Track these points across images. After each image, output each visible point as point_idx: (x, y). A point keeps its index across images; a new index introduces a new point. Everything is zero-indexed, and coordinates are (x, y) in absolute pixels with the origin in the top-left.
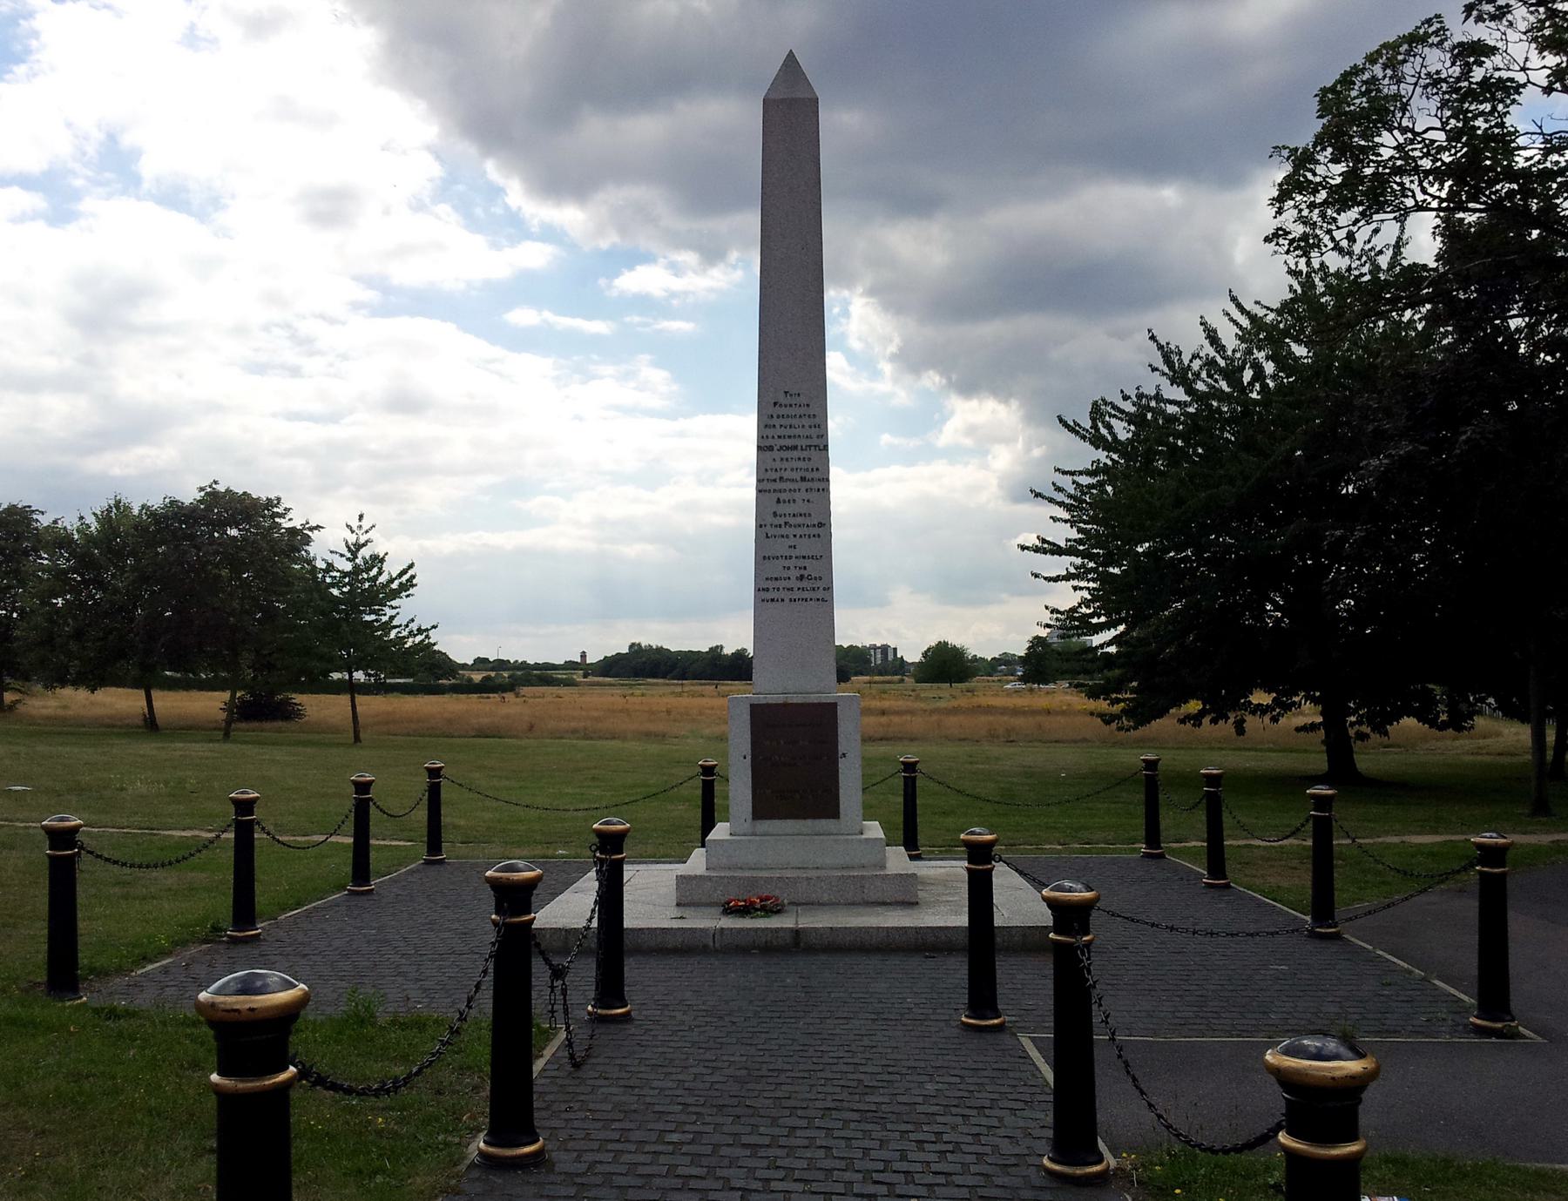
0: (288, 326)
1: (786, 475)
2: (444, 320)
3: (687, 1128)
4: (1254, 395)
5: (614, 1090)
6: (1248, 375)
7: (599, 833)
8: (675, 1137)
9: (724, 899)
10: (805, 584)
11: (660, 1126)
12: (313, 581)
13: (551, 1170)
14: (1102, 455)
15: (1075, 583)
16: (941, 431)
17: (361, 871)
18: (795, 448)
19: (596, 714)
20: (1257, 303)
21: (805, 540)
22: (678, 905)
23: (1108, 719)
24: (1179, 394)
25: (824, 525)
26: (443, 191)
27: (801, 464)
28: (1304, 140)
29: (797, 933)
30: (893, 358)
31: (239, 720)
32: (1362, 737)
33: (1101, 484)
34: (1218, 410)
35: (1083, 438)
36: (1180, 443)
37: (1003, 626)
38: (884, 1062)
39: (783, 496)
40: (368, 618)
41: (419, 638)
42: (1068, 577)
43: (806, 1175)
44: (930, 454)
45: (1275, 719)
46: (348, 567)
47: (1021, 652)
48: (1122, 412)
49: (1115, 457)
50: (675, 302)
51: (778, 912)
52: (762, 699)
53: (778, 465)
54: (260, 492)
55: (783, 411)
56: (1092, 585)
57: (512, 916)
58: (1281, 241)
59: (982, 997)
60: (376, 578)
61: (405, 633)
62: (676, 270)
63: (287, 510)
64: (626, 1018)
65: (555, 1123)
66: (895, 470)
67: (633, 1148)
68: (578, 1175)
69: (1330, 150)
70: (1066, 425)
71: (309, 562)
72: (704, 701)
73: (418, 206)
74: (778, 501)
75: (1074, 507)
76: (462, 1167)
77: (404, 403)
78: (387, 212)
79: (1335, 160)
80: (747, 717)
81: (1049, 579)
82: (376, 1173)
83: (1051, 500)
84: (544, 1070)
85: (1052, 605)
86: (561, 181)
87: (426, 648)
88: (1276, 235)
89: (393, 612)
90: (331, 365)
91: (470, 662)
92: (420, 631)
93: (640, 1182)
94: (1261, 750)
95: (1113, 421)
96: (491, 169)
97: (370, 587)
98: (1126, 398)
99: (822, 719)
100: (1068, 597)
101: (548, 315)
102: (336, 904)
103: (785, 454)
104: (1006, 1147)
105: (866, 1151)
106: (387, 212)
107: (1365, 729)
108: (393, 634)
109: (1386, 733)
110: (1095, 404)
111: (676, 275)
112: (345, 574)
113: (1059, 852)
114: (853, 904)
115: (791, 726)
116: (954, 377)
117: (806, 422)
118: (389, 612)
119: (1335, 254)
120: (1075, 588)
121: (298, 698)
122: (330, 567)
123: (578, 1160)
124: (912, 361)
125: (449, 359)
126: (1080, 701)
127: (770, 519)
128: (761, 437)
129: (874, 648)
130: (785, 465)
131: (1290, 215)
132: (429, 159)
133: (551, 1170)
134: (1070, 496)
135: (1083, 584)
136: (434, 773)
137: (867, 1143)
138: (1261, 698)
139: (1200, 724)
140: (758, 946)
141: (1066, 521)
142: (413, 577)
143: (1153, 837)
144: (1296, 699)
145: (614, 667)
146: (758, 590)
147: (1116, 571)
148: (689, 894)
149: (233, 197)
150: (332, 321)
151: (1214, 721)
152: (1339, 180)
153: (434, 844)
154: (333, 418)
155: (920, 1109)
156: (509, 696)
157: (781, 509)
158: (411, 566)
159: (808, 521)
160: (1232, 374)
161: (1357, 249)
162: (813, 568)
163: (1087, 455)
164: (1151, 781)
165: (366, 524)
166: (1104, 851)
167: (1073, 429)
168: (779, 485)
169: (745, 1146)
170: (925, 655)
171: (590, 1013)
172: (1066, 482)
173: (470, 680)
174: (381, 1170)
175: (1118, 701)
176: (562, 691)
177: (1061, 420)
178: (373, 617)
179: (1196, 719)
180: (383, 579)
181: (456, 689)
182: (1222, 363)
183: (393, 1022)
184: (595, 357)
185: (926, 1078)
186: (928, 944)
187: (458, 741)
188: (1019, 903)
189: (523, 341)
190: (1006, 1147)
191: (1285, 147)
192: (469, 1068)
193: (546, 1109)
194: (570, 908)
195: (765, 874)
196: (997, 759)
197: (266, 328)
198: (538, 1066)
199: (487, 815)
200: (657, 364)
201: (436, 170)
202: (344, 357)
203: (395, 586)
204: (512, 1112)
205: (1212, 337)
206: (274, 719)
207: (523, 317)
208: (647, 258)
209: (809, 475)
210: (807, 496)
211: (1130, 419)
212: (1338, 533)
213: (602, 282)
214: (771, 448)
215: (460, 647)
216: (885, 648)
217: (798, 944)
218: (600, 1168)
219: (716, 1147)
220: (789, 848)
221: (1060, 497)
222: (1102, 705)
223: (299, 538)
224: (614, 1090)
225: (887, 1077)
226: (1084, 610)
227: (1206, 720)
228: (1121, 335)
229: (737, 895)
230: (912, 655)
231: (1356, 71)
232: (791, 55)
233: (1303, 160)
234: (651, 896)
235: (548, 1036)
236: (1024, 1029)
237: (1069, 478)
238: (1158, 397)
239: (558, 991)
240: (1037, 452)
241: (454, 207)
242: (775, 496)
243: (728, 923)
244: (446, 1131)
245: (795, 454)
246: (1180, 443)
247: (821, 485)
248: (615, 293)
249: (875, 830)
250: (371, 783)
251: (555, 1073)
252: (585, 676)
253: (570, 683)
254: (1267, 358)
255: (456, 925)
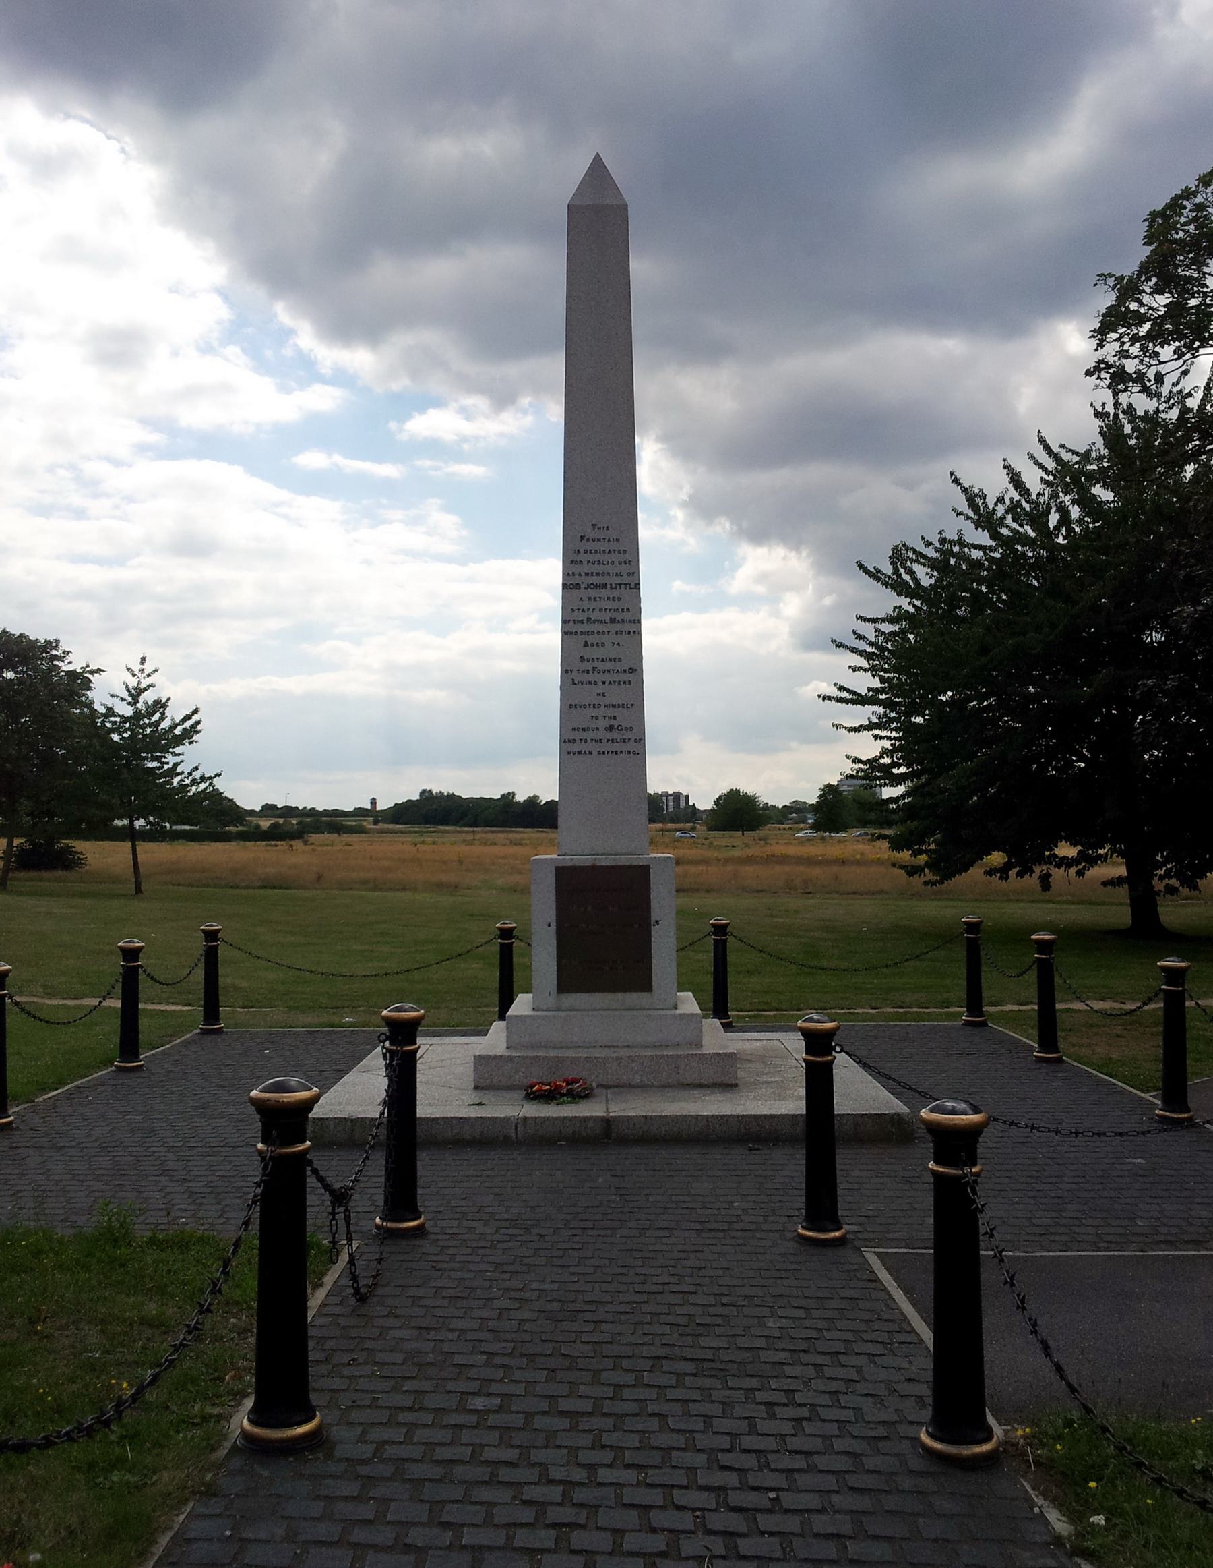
0: (72, 467)
2: (231, 462)
3: (495, 1388)
4: (1060, 540)
5: (404, 1333)
6: (1054, 519)
7: (389, 1022)
8: (479, 1403)
9: (527, 1082)
11: (462, 1386)
12: (93, 725)
13: (329, 1456)
14: (904, 602)
15: (877, 732)
16: (733, 578)
17: (130, 1044)
18: (604, 586)
19: (386, 863)
20: (1062, 446)
22: (476, 1088)
23: (912, 871)
24: (984, 538)
25: (636, 670)
26: (233, 332)
27: (609, 604)
28: (1129, 268)
29: (607, 1122)
30: (684, 505)
31: (17, 869)
32: (1171, 890)
33: (903, 632)
34: (1024, 555)
35: (885, 584)
36: (984, 589)
37: (793, 775)
38: (716, 1289)
39: (590, 639)
40: (150, 765)
41: (203, 786)
42: (871, 726)
43: (639, 1458)
44: (723, 601)
45: (1080, 873)
46: (128, 711)
47: (813, 800)
48: (925, 557)
49: (918, 603)
50: (466, 447)
51: (586, 1097)
52: (568, 861)
53: (586, 604)
54: (38, 634)
55: (590, 546)
56: (894, 734)
57: (283, 1145)
58: (1103, 375)
59: (821, 1204)
60: (158, 723)
61: (187, 782)
62: (467, 414)
63: (67, 653)
64: (420, 1231)
65: (337, 1383)
66: (686, 617)
67: (428, 1418)
68: (363, 1462)
69: (1154, 280)
70: (866, 571)
71: (89, 705)
72: (495, 850)
73: (206, 349)
74: (586, 644)
75: (876, 658)
76: (222, 1453)
77: (191, 546)
78: (175, 353)
79: (1158, 290)
80: (551, 880)
81: (851, 730)
82: (113, 1467)
83: (853, 650)
84: (323, 1305)
85: (854, 754)
86: (348, 325)
87: (216, 796)
88: (1097, 369)
89: (177, 759)
90: (117, 507)
91: (258, 809)
92: (203, 779)
93: (438, 1472)
94: (1059, 902)
95: (916, 567)
96: (283, 313)
97: (152, 734)
98: (928, 544)
99: (634, 882)
100: (869, 747)
101: (337, 458)
102: (102, 1083)
103: (592, 593)
104: (872, 1412)
105: (707, 1419)
106: (175, 353)
107: (1174, 882)
108: (176, 781)
109: (1196, 888)
110: (895, 548)
111: (467, 419)
112: (125, 719)
113: (872, 1018)
114: (668, 1086)
115: (588, 881)
116: (745, 524)
117: (615, 557)
118: (171, 760)
119: (1143, 396)
120: (876, 737)
121: (79, 845)
122: (110, 712)
123: (362, 1439)
124: (703, 508)
125: (237, 502)
126: (882, 849)
127: (577, 664)
128: (566, 574)
129: (666, 795)
130: (593, 605)
131: (1111, 348)
132: (217, 301)
133: (329, 1456)
134: (871, 644)
135: (884, 733)
136: (211, 936)
137: (707, 1408)
138: (1066, 850)
139: (1007, 878)
140: (569, 1141)
141: (865, 670)
142: (198, 723)
143: (974, 1003)
144: (1101, 852)
145: (404, 814)
146: (564, 741)
147: (919, 720)
148: (488, 1078)
149: (21, 336)
150: (117, 463)
151: (1020, 874)
152: (1162, 311)
153: (211, 1012)
154: (119, 560)
155: (764, 1356)
156: (297, 844)
157: (589, 653)
158: (196, 711)
159: (618, 667)
160: (1037, 517)
161: (1165, 391)
162: (623, 718)
163: (887, 602)
164: (973, 942)
165: (148, 668)
166: (918, 1018)
167: (875, 575)
169: (563, 1414)
170: (717, 802)
171: (378, 1227)
172: (869, 630)
173: (258, 826)
174: (119, 1463)
175: (921, 852)
176: (353, 838)
177: (860, 566)
178: (155, 764)
179: (1003, 872)
180: (165, 725)
181: (243, 837)
182: (1027, 507)
183: (153, 1241)
184: (385, 501)
185: (766, 1312)
186: (755, 1135)
187: (244, 892)
188: (857, 1091)
189: (313, 484)
190: (872, 1412)
191: (1110, 275)
192: (237, 1303)
193: (326, 1361)
194: (360, 1092)
195: (571, 1054)
196: (796, 912)
197: (51, 469)
198: (316, 1299)
199: (271, 976)
200: (447, 509)
201: (224, 312)
202: (130, 499)
203: (178, 731)
204: (283, 1383)
205: (1016, 480)
206: (54, 868)
207: (313, 460)
208: (438, 403)
209: (619, 617)
211: (932, 564)
212: (1151, 682)
213: (393, 425)
215: (248, 793)
216: (677, 796)
217: (609, 1134)
218: (390, 1451)
219: (529, 1415)
220: (598, 1025)
221: (862, 646)
222: (905, 856)
223: (79, 681)
224: (404, 1333)
225: (720, 1310)
226: (886, 760)
227: (1013, 873)
228: (910, 485)
229: (536, 1075)
230: (704, 802)
231: (1187, 194)
232: (597, 160)
233: (1128, 289)
234: (447, 1073)
235: (332, 1255)
236: (868, 1242)
237: (871, 626)
238: (961, 543)
239: (340, 1217)
240: (828, 601)
241: (244, 350)
242: (582, 639)
243: (532, 1110)
244: (206, 1398)
246: (984, 589)
247: (632, 628)
248: (404, 437)
249: (689, 1004)
250: (139, 949)
251: (337, 1310)
252: (375, 823)
253: (360, 830)
254: (1073, 504)
255: (231, 1110)
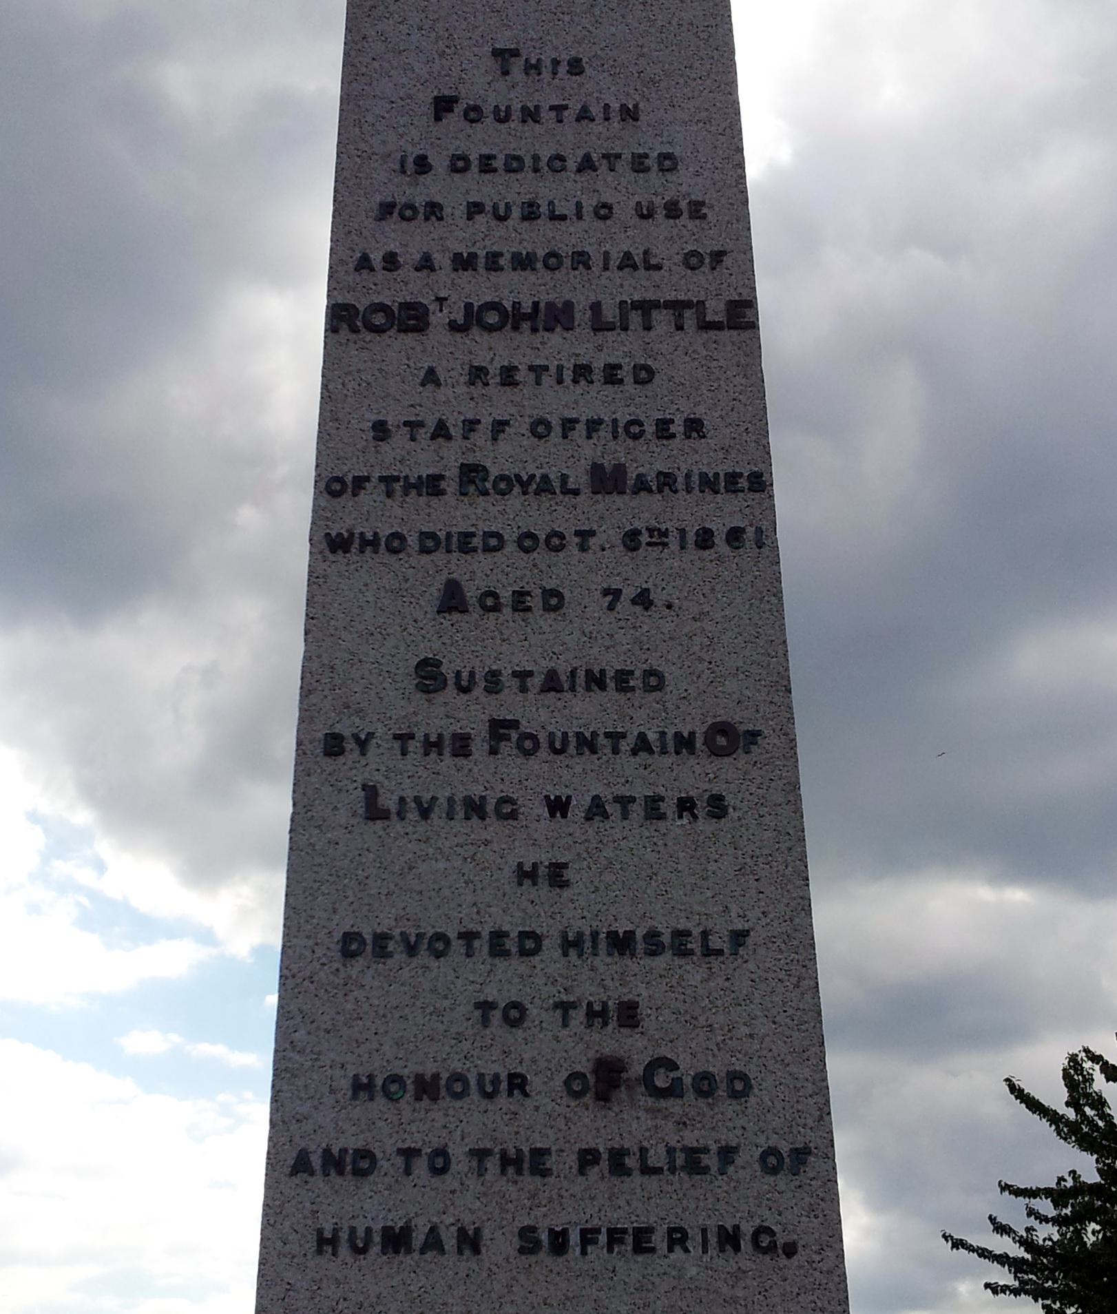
1: (501, 458)
10: (633, 1123)
18: (557, 317)
21: (626, 833)
39: (477, 573)
53: (455, 402)
74: (452, 600)
83: (984, 1253)
130: (497, 403)
157: (468, 645)
159: (644, 716)
162: (681, 1015)
168: (454, 513)
172: (1014, 1213)
209: (647, 459)
210: (636, 572)
214: (412, 319)
242: (428, 574)
245: (558, 348)
